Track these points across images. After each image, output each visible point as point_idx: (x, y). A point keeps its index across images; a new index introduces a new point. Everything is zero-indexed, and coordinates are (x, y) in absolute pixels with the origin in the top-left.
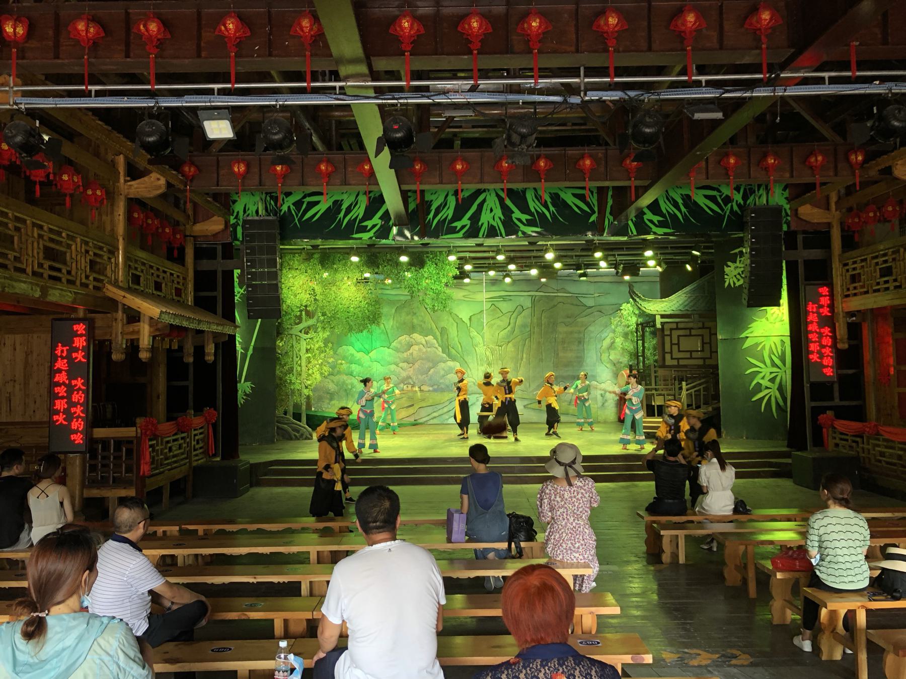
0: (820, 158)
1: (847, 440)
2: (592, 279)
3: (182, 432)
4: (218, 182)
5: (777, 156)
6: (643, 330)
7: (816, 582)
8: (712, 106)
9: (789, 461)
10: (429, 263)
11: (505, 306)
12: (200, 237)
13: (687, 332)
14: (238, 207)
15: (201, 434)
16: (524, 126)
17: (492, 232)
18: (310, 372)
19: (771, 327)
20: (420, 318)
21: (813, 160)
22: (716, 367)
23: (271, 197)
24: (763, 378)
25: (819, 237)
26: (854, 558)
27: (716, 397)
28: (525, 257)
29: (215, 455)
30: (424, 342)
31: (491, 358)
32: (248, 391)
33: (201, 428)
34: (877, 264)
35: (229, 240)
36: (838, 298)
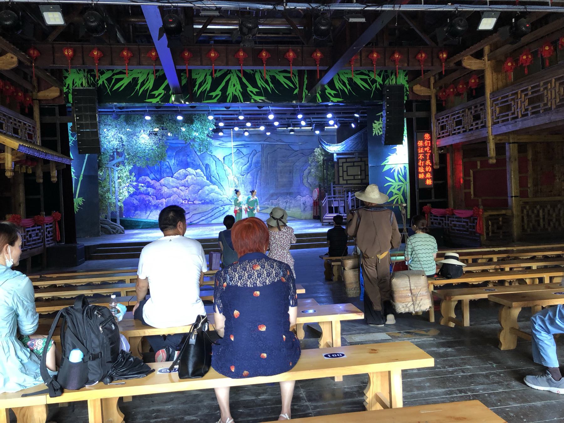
0: (423, 55)
1: (437, 220)
3: (38, 226)
4: (54, 61)
6: (327, 164)
8: (360, 15)
11: (245, 151)
12: (42, 100)
13: (352, 164)
14: (69, 81)
15: (50, 227)
16: (250, 23)
17: (235, 99)
18: (121, 191)
19: (398, 158)
20: (192, 158)
21: (420, 56)
23: (91, 75)
24: (394, 188)
25: (424, 104)
26: (428, 259)
28: (257, 118)
29: (60, 242)
30: (195, 174)
31: (237, 182)
32: (81, 203)
33: (50, 224)
34: (454, 118)
35: (63, 103)
36: (434, 139)
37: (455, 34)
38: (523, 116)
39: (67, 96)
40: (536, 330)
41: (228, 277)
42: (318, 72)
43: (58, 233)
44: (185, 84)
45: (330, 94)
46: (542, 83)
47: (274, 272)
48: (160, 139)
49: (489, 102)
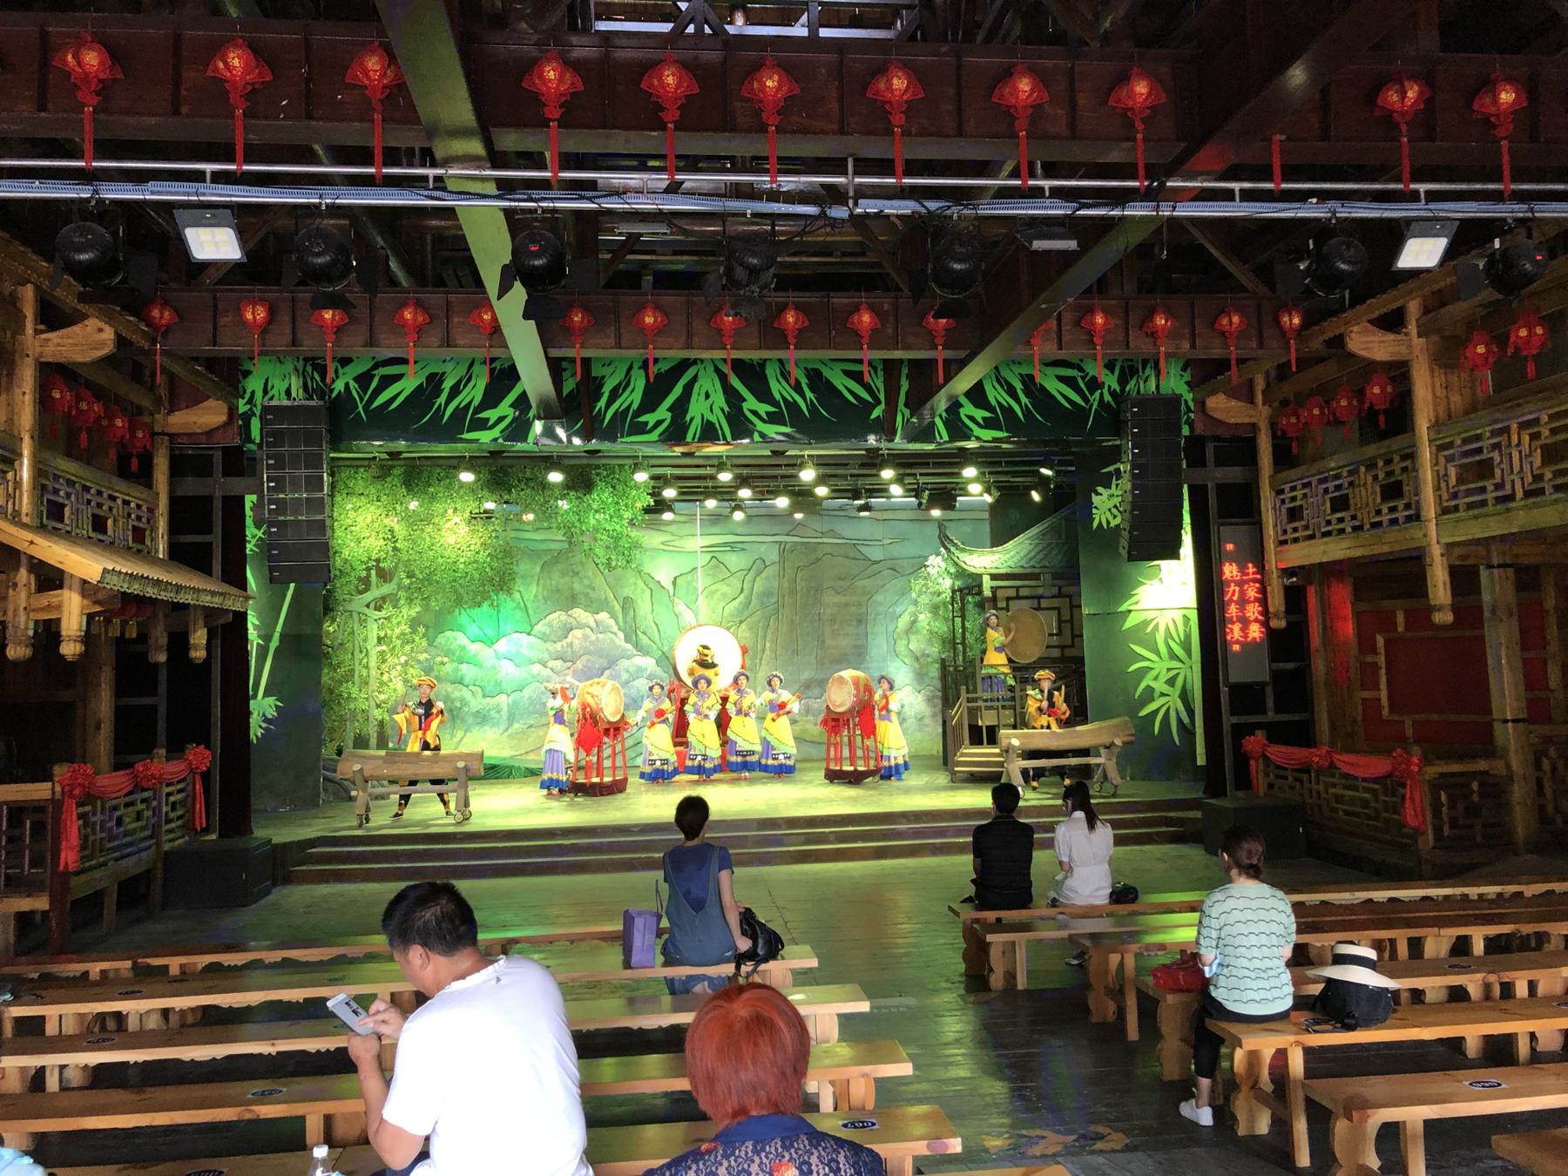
0: (1236, 319)
4: (215, 336)
5: (1170, 314)
6: (962, 600)
8: (1062, 230)
10: (601, 485)
11: (734, 561)
12: (179, 435)
14: (254, 384)
15: (179, 791)
16: (755, 255)
17: (709, 433)
18: (385, 678)
19: (1165, 595)
20: (586, 582)
21: (1225, 321)
22: (1081, 661)
24: (1156, 678)
25: (1240, 447)
28: (768, 476)
29: (206, 830)
30: (593, 624)
32: (271, 713)
35: (237, 441)
38: (1528, 494)
39: (247, 426)
42: (940, 364)
43: (200, 806)
45: (972, 418)
49: (1426, 453)
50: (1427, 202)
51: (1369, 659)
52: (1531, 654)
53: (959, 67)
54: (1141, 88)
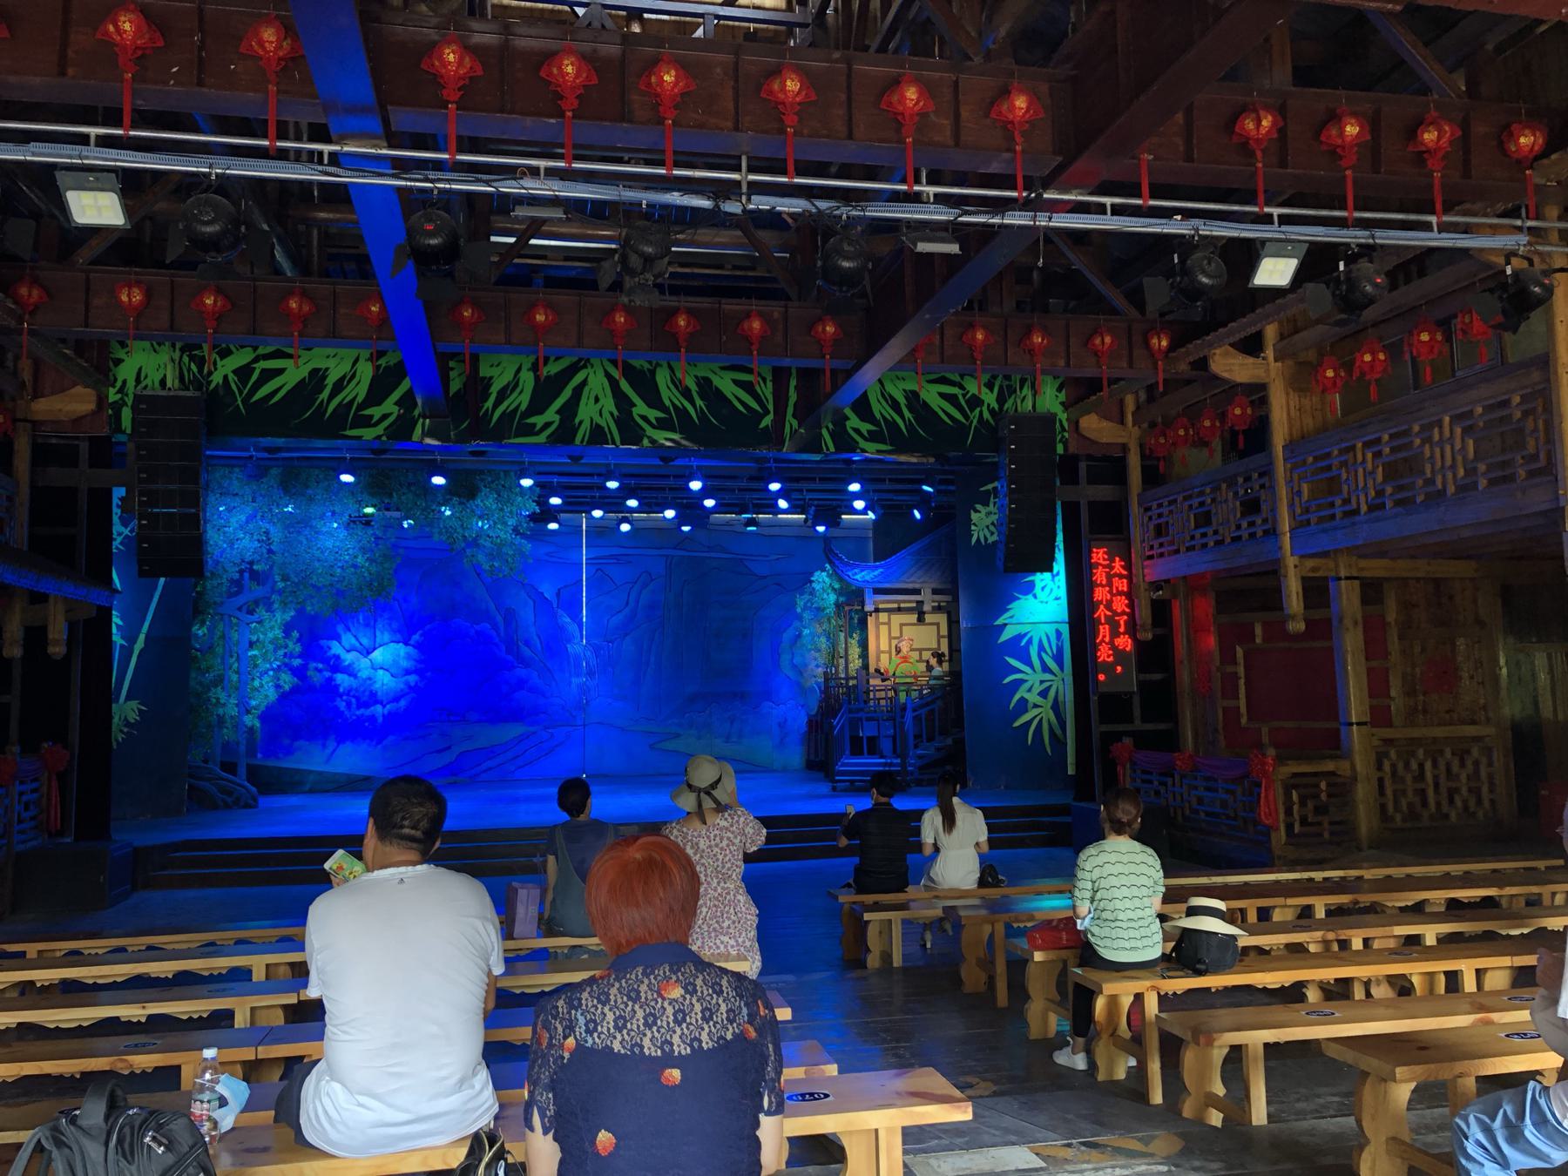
0: (1108, 340)
2: (766, 531)
4: (87, 317)
5: (1046, 333)
7: (1087, 954)
8: (944, 234)
9: (1068, 819)
10: (485, 491)
12: (43, 423)
14: (126, 372)
15: (33, 791)
16: (650, 243)
19: (1042, 606)
21: (1098, 341)
23: (192, 358)
24: (1029, 690)
25: (1111, 466)
26: (1140, 913)
27: (959, 722)
32: (133, 717)
35: (105, 432)
37: (1194, 293)
38: (1371, 509)
39: (117, 416)
40: (1469, 1158)
41: (582, 1020)
44: (459, 391)
46: (1416, 428)
47: (723, 1008)
48: (377, 538)
50: (1280, 224)
51: (1230, 669)
52: (1374, 664)
53: (849, 76)
54: (1021, 102)
